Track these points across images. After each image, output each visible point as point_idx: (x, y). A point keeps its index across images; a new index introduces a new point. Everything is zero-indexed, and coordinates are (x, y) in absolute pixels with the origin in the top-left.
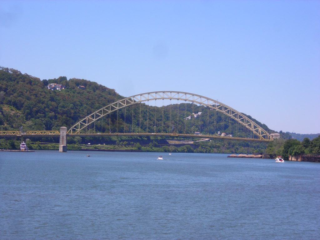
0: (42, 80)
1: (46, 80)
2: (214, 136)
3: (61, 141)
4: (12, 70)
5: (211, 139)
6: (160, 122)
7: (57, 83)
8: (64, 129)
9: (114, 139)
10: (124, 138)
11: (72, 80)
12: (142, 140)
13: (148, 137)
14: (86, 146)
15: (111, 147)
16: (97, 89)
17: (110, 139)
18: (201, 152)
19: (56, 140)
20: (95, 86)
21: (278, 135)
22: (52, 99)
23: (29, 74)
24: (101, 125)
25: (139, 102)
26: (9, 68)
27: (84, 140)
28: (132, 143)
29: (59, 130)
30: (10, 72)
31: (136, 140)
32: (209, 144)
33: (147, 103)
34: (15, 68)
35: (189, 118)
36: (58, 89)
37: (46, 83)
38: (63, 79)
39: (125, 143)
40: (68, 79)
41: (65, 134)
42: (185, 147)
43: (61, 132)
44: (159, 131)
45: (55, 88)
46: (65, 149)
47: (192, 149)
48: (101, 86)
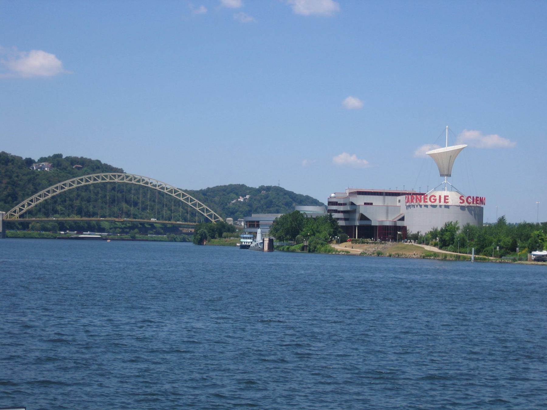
0: (24, 158)
11: (67, 158)
20: (99, 165)
36: (46, 169)
37: (29, 162)
38: (58, 157)
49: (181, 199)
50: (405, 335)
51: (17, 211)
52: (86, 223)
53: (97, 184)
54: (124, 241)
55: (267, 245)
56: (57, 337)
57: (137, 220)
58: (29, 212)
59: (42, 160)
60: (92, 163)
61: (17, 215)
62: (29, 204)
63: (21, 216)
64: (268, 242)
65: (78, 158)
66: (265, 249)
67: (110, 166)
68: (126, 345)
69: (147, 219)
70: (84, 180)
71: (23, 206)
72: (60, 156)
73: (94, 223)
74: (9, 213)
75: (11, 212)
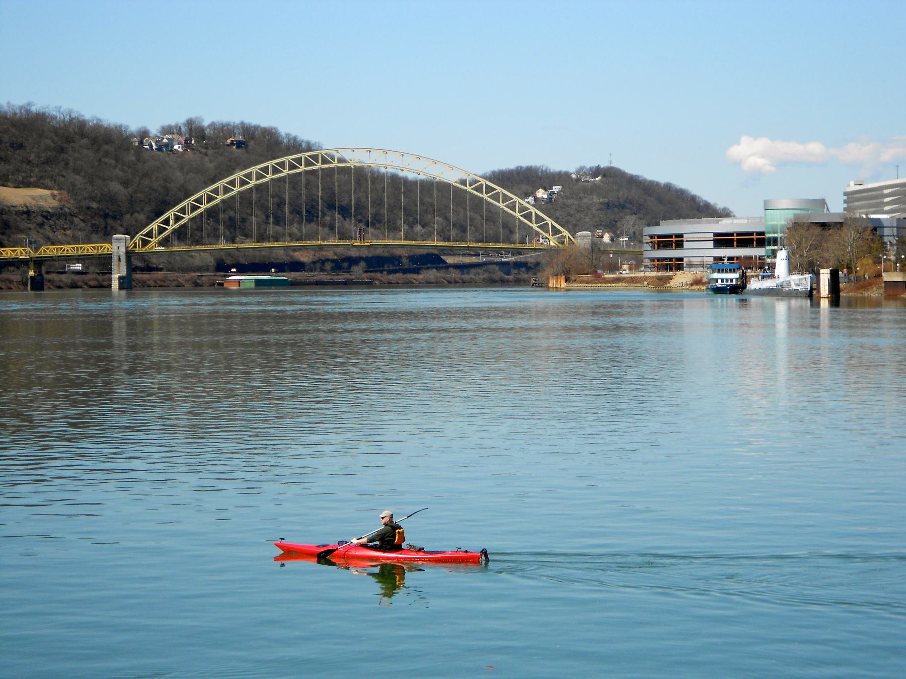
8: (118, 240)
36: (176, 147)
41: (123, 250)
49: (485, 196)
50: (325, 335)
51: (154, 232)
55: (827, 283)
58: (180, 234)
59: (167, 130)
62: (178, 219)
63: (165, 242)
64: (829, 276)
66: (822, 291)
68: (619, 567)
70: (237, 182)
71: (166, 222)
75: (141, 235)
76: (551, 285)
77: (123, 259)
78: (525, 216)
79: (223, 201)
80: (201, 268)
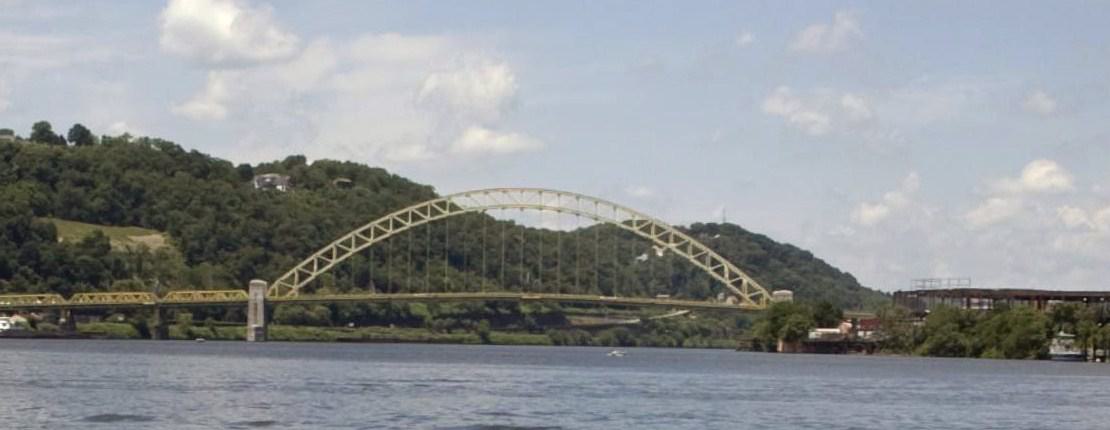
0: (236, 165)
1: (248, 166)
2: (707, 303)
3: (250, 316)
4: (157, 142)
5: (699, 310)
6: (552, 270)
7: (279, 172)
8: (258, 285)
9: (418, 309)
10: (446, 308)
11: (318, 164)
12: (498, 315)
13: (512, 305)
14: (343, 331)
15: (413, 333)
16: (384, 185)
17: (406, 309)
18: (655, 345)
19: (240, 313)
20: (380, 180)
21: (788, 295)
22: (258, 214)
23: (202, 150)
24: (387, 278)
25: (480, 211)
26: (151, 137)
27: (336, 316)
28: (468, 321)
29: (247, 289)
30: (153, 146)
31: (476, 315)
32: (684, 324)
33: (490, 212)
34: (167, 138)
35: (644, 257)
36: (279, 187)
37: (246, 172)
38: (296, 161)
39: (449, 321)
40: (309, 163)
41: (260, 297)
42: (609, 334)
43: (252, 291)
44: (548, 290)
45: (272, 185)
46: (263, 335)
47: (631, 336)
48: (396, 177)
52: (359, 306)
53: (421, 228)
54: (399, 345)
56: (642, 387)
57: (553, 296)
60: (753, 271)
61: (296, 287)
63: (308, 289)
65: (339, 163)
67: (405, 180)
69: (487, 292)
72: (301, 159)
73: (399, 305)
74: (275, 286)
76: (1052, 351)
77: (261, 308)
78: (699, 259)
79: (374, 245)
80: (224, 312)
